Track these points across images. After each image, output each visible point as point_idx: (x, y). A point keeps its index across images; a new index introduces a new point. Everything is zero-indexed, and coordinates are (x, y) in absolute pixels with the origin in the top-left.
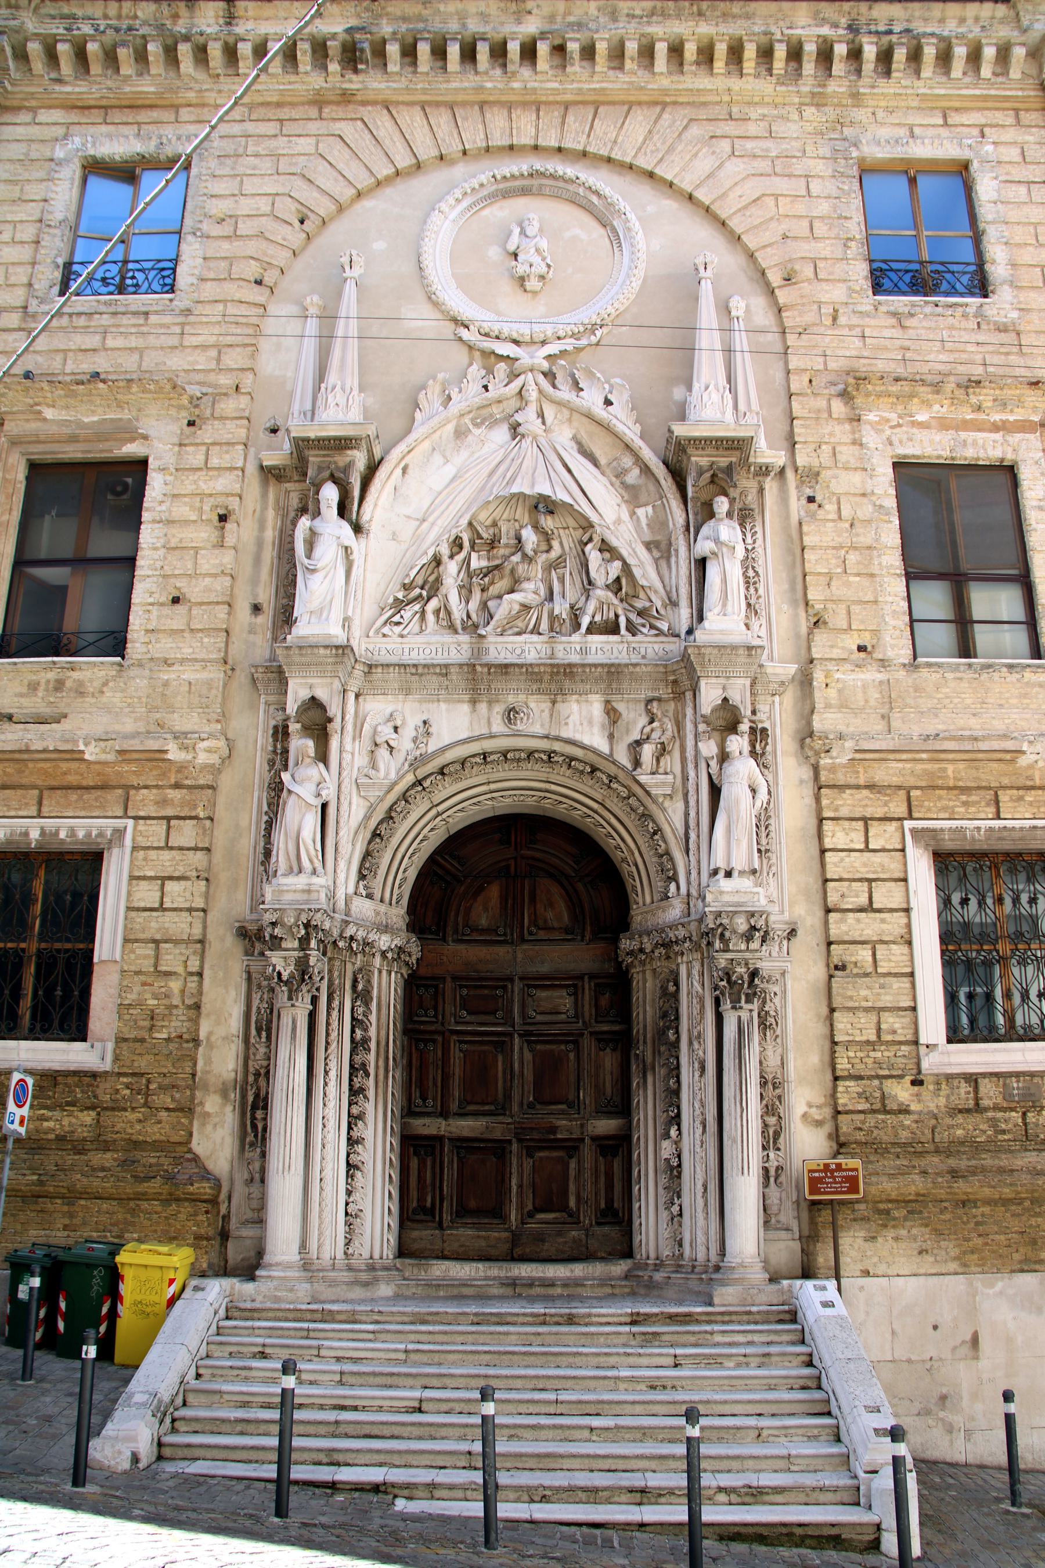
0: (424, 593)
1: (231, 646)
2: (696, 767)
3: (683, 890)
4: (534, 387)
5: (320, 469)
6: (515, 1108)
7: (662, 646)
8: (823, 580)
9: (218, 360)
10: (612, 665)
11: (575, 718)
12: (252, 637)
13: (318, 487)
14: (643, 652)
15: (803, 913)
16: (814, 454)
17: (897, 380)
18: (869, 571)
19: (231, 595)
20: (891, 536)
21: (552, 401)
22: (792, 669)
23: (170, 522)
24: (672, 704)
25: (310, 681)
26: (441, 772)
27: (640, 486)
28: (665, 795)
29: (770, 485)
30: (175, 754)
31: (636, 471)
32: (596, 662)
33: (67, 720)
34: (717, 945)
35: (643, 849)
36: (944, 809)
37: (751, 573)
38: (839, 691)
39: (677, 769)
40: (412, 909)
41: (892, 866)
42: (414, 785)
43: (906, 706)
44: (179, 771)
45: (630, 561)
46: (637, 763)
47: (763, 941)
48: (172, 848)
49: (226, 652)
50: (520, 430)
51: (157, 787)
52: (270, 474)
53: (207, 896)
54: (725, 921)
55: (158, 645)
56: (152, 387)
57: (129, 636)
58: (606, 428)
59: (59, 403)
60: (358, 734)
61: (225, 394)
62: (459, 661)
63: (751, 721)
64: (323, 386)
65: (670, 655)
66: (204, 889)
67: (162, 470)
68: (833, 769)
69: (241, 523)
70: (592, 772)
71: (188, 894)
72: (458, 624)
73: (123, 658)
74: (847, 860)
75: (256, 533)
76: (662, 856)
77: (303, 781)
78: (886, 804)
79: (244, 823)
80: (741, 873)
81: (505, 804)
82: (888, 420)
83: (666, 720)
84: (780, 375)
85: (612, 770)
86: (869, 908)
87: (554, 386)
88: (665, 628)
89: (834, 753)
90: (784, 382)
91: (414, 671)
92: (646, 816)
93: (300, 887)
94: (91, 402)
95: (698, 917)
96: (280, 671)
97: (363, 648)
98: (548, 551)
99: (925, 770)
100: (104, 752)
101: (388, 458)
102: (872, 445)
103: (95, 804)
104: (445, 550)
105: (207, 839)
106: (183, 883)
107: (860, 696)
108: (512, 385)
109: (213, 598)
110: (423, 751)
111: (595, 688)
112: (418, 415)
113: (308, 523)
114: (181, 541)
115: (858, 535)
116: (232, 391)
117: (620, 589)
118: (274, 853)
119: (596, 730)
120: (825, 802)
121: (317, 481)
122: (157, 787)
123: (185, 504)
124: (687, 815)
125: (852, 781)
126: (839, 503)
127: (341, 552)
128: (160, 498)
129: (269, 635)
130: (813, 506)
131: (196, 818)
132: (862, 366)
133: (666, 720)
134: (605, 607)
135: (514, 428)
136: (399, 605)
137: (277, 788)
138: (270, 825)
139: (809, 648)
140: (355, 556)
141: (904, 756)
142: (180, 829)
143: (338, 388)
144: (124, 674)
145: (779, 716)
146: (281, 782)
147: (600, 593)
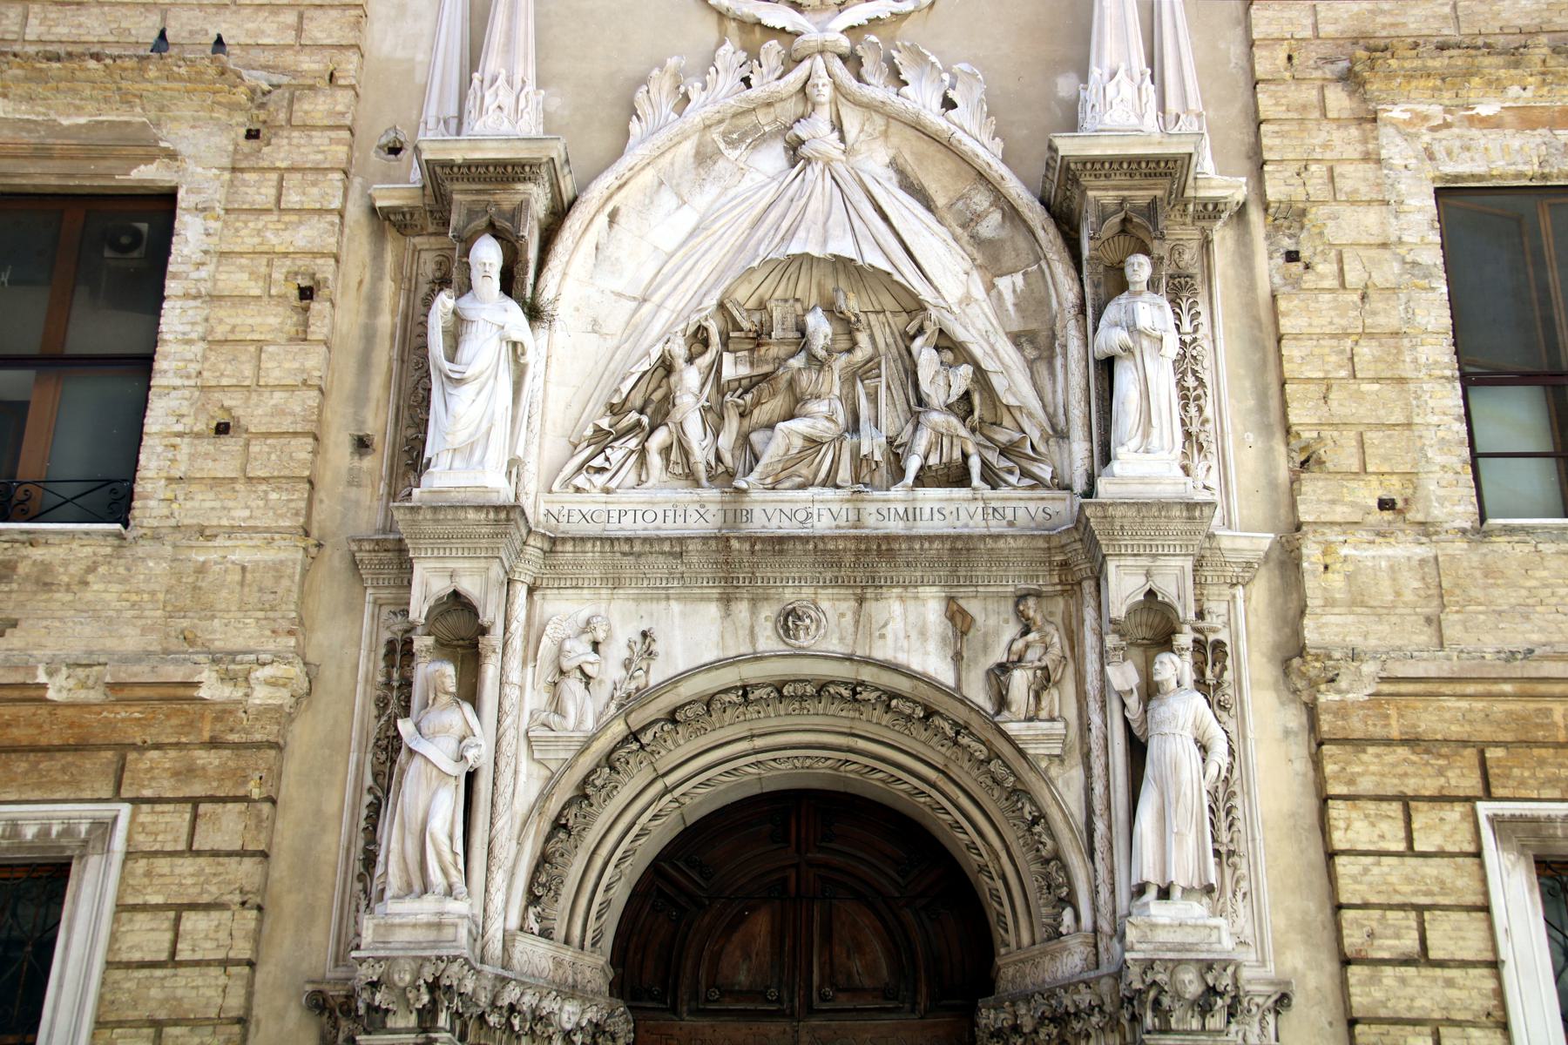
0: (645, 420)
1: (317, 507)
2: (1103, 707)
3: (1086, 921)
4: (826, 79)
5: (472, 214)
7: (1042, 505)
8: (1315, 391)
9: (299, 30)
10: (958, 537)
11: (896, 626)
12: (353, 493)
13: (467, 243)
14: (1010, 516)
15: (1300, 965)
16: (1296, 181)
17: (1442, 47)
18: (1397, 373)
19: (319, 421)
20: (1433, 312)
21: (857, 103)
22: (1265, 540)
23: (214, 298)
24: (1061, 602)
25: (451, 564)
26: (672, 718)
27: (1002, 241)
28: (1050, 756)
29: (1222, 236)
30: (212, 689)
31: (996, 217)
32: (932, 532)
33: (17, 632)
34: (1149, 1020)
35: (1015, 849)
36: (1552, 781)
37: (1190, 382)
38: (1348, 577)
39: (1071, 712)
40: (621, 955)
41: (1460, 883)
42: (625, 741)
43: (1470, 601)
44: (218, 719)
45: (987, 364)
46: (1002, 702)
47: (1231, 1015)
48: (199, 853)
49: (309, 516)
50: (805, 150)
51: (178, 745)
52: (386, 221)
53: (257, 937)
54: (1161, 977)
55: (189, 504)
56: (183, 71)
57: (137, 489)
58: (947, 146)
59: (15, 90)
60: (531, 654)
61: (311, 87)
62: (702, 533)
63: (1196, 630)
64: (476, 76)
65: (1055, 520)
66: (253, 924)
67: (202, 210)
68: (1342, 711)
69: (338, 301)
70: (927, 717)
71: (223, 936)
72: (701, 470)
73: (126, 525)
74: (1375, 870)
75: (362, 319)
76: (1047, 862)
77: (434, 734)
78: (1441, 772)
79: (331, 807)
80: (1187, 891)
81: (779, 773)
82: (1426, 118)
83: (1050, 629)
84: (1236, 51)
85: (961, 714)
86: (1421, 958)
87: (860, 79)
88: (1048, 477)
89: (1343, 683)
90: (1243, 63)
91: (626, 548)
92: (1019, 792)
93: (424, 918)
94: (75, 91)
95: (1113, 969)
96: (400, 549)
97: (542, 511)
98: (849, 351)
99: (1510, 713)
100: (83, 685)
101: (585, 197)
102: (1398, 162)
103: (60, 777)
104: (679, 349)
105: (263, 837)
106: (215, 915)
107: (1386, 585)
108: (790, 77)
109: (287, 425)
110: (641, 682)
111: (929, 576)
112: (635, 127)
113: (451, 303)
114: (233, 330)
115: (1374, 313)
116: (323, 83)
117: (971, 412)
118: (381, 858)
119: (932, 646)
120: (1330, 768)
121: (466, 234)
122: (178, 745)
123: (241, 268)
124: (1089, 790)
125: (1378, 732)
126: (1340, 261)
127: (506, 351)
128: (198, 257)
129: (383, 488)
130: (1296, 268)
131: (245, 799)
132: (1380, 27)
133: (1050, 629)
134: (946, 441)
135: (795, 150)
136: (602, 439)
137: (389, 749)
138: (375, 811)
139: (1293, 506)
140: (529, 358)
141: (1471, 689)
142: (215, 819)
143: (501, 81)
144: (127, 553)
145: (1245, 620)
146: (398, 736)
147: (937, 418)
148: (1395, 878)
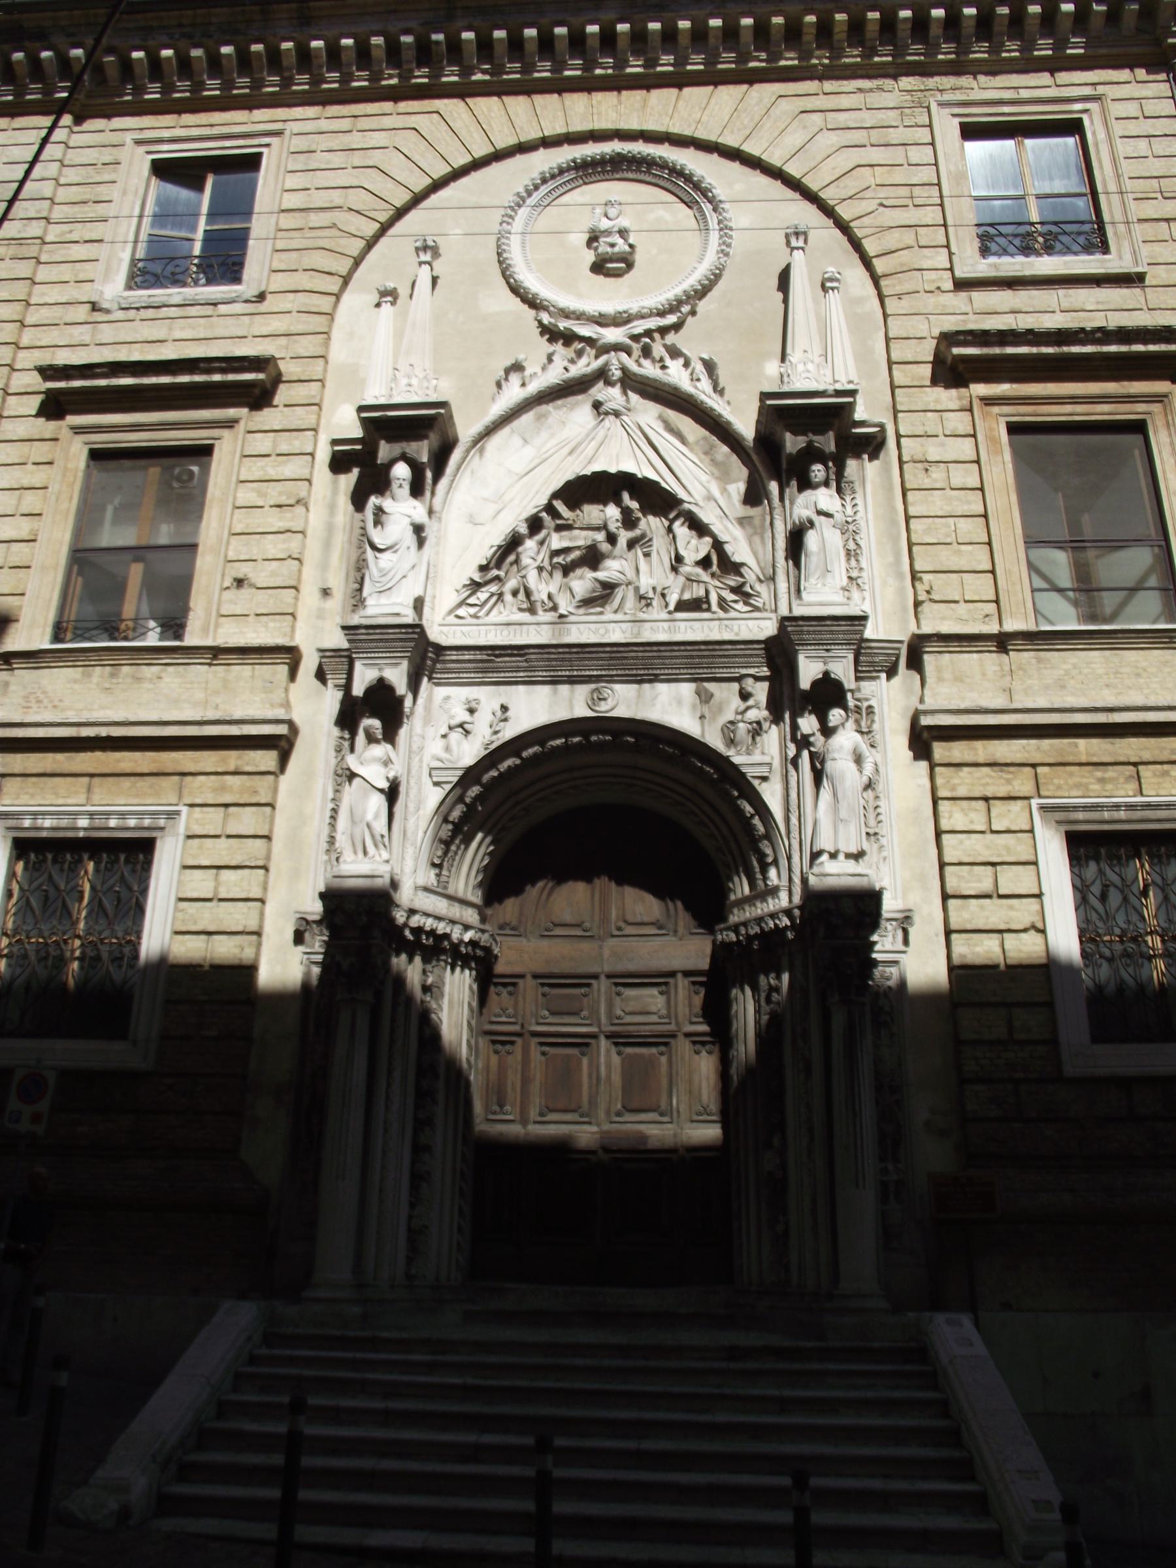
6: (602, 1114)
45: (723, 537)
78: (1009, 782)
104: (523, 529)
136: (475, 586)
148: (978, 847)
